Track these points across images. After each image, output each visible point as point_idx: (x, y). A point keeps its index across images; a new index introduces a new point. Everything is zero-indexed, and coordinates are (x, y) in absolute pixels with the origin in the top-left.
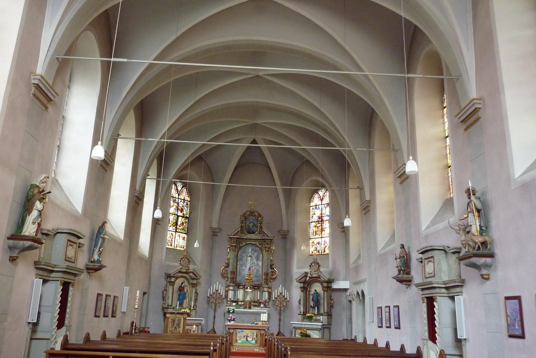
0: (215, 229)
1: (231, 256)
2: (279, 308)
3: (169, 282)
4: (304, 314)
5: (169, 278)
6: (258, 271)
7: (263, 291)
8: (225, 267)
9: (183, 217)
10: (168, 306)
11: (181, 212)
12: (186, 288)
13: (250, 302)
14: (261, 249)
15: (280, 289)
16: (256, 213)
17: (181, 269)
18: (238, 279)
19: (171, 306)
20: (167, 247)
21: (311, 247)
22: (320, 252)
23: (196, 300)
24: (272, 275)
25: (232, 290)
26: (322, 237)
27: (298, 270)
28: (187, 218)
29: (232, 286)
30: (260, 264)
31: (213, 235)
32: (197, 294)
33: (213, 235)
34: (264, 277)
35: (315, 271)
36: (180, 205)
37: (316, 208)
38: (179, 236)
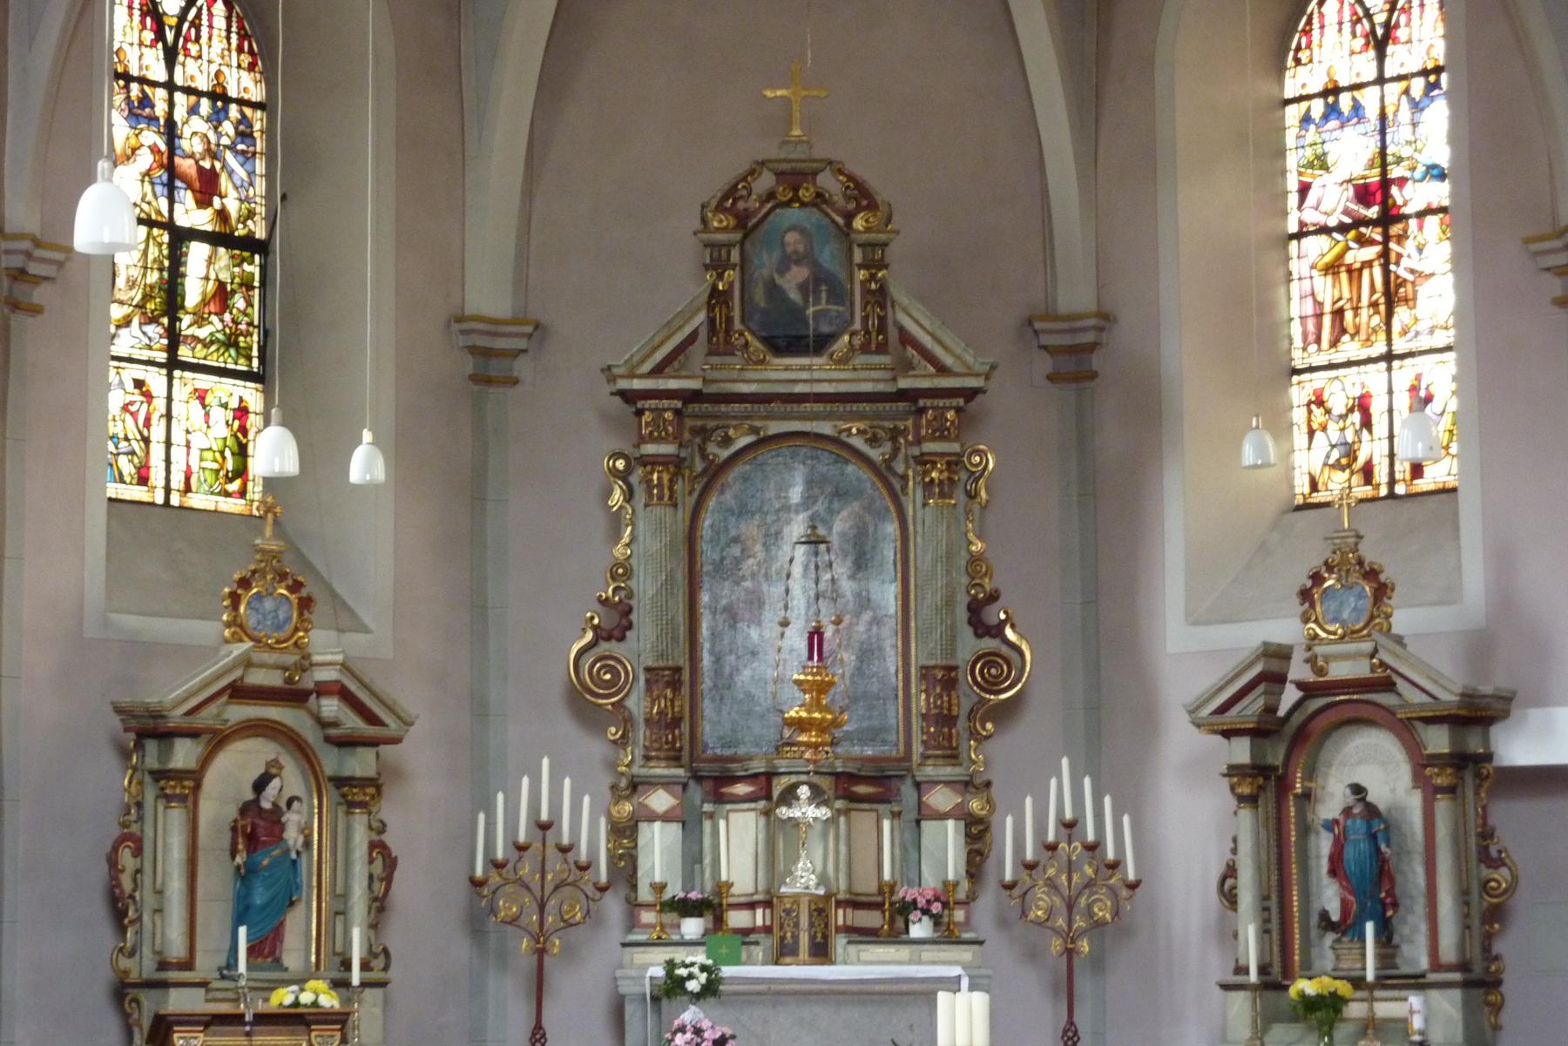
0: (494, 325)
1: (646, 540)
2: (1056, 945)
3: (159, 775)
4: (1272, 983)
5: (151, 746)
6: (867, 653)
7: (924, 814)
8: (601, 635)
9: (214, 239)
10: (163, 965)
11: (203, 202)
12: (292, 820)
13: (820, 909)
14: (882, 472)
15: (1062, 790)
16: (829, 182)
17: (247, 663)
18: (715, 725)
19: (188, 965)
20: (114, 490)
21: (1300, 437)
22: (1381, 474)
23: (380, 906)
24: (993, 686)
25: (666, 818)
26: (1389, 357)
27: (1197, 640)
28: (249, 245)
29: (666, 784)
30: (887, 595)
31: (482, 379)
32: (391, 864)
33: (482, 379)
34: (920, 702)
35: (1349, 635)
36: (190, 143)
37: (1332, 111)
38: (201, 396)
